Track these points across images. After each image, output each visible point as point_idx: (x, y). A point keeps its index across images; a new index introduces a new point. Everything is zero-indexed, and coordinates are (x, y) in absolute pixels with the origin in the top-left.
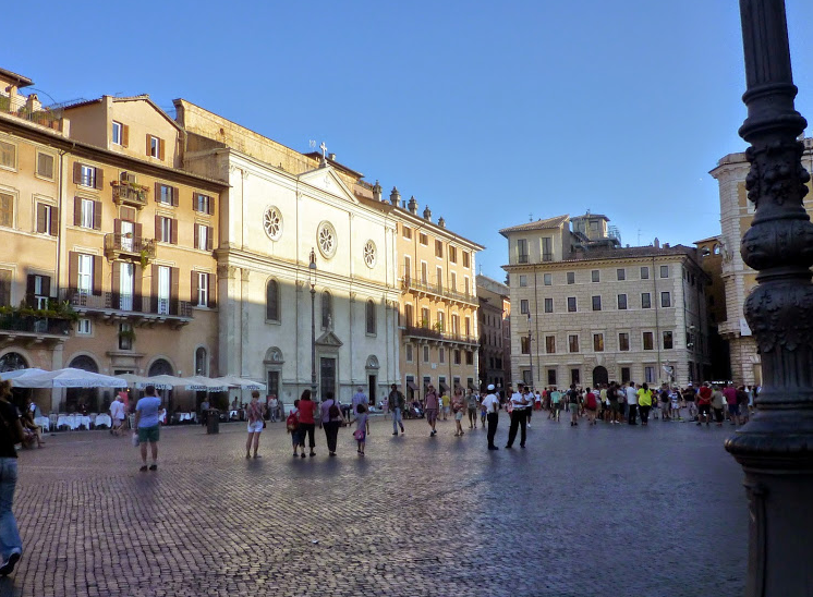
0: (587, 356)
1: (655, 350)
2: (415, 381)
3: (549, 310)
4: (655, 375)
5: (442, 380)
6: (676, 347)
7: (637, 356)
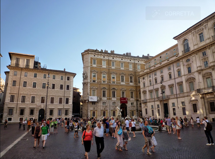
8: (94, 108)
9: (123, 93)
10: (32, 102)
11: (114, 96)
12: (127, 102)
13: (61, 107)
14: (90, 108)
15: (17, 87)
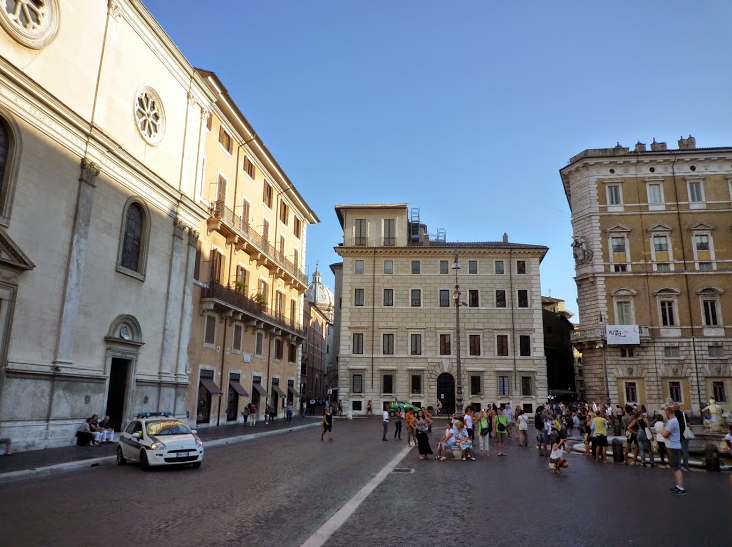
0: (433, 361)
1: (511, 356)
2: (216, 380)
3: (388, 302)
4: (510, 388)
5: (257, 380)
6: (534, 354)
7: (489, 363)
8: (631, 371)
10: (414, 352)
14: (614, 371)
15: (368, 306)
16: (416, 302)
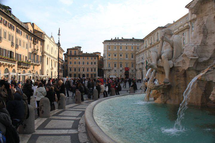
9: (127, 64)
11: (121, 66)
12: (129, 70)
13: (92, 73)
16: (88, 64)
